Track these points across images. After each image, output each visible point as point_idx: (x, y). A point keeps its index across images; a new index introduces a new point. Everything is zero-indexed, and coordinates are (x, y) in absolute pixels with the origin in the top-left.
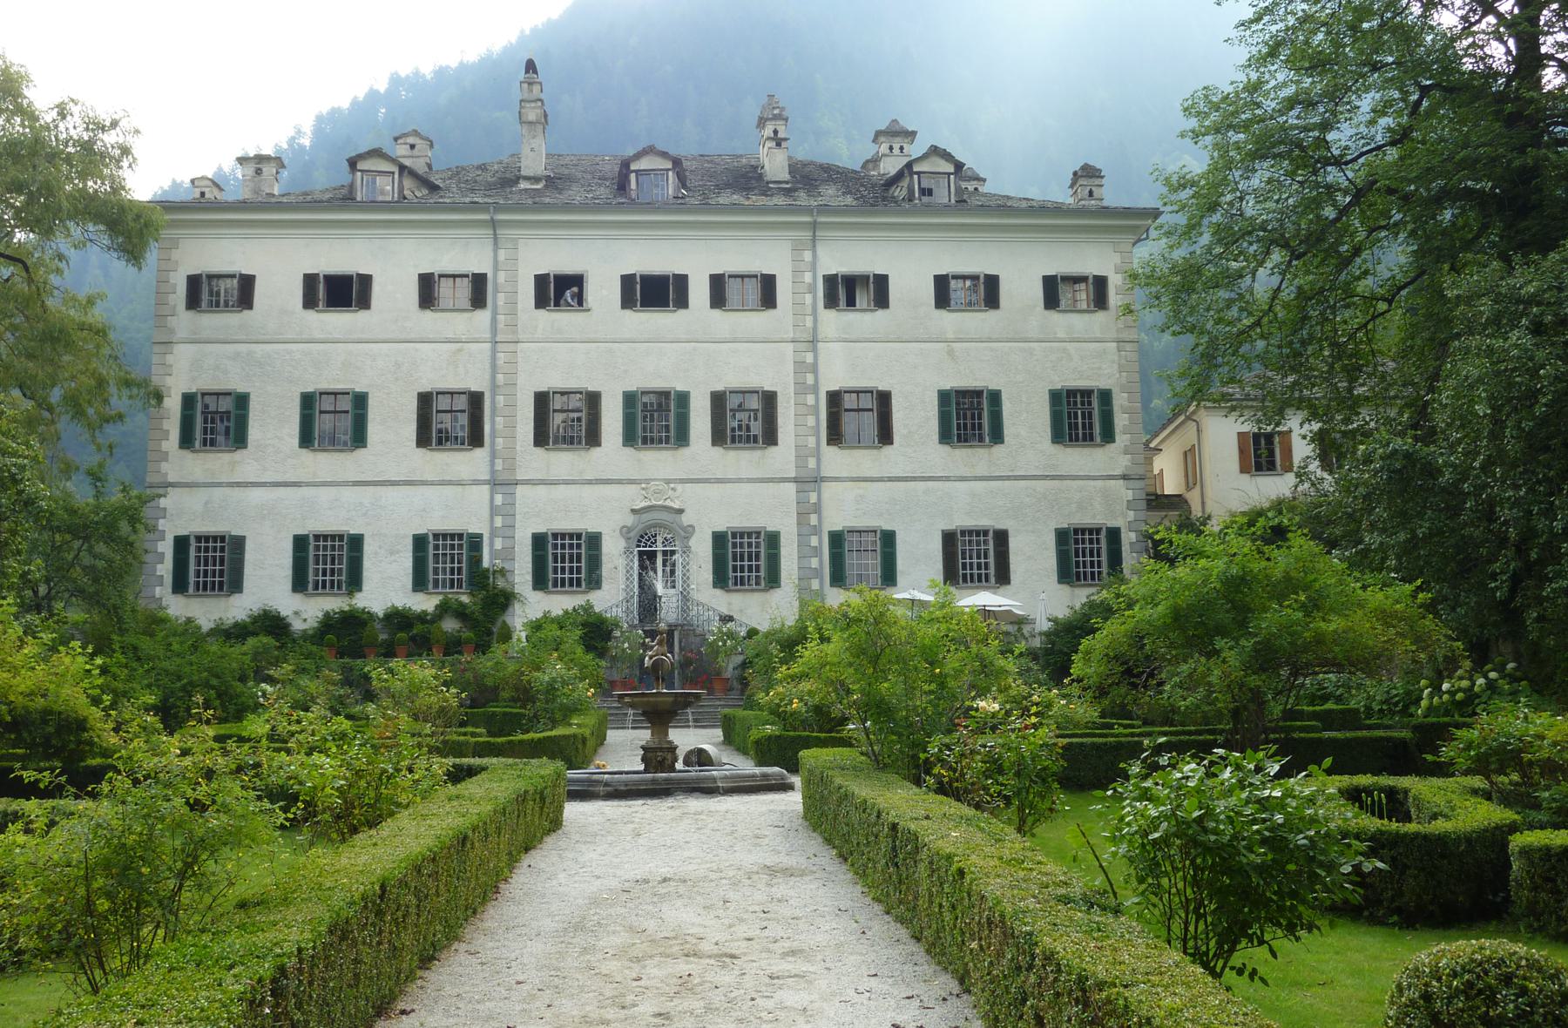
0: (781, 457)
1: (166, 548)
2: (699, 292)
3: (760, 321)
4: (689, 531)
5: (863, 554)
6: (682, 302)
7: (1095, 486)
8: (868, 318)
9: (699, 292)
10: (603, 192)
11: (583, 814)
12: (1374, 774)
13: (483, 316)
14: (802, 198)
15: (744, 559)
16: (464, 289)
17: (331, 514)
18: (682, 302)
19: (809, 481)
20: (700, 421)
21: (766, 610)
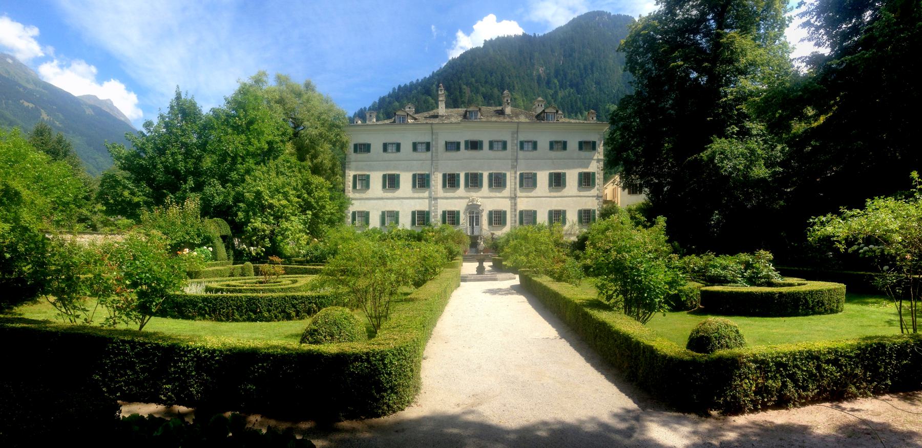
0: (507, 192)
1: (350, 215)
2: (486, 145)
3: (502, 154)
4: (483, 210)
5: (528, 217)
6: (481, 148)
7: (590, 201)
8: (531, 153)
9: (486, 145)
10: (460, 119)
11: (727, 326)
12: (319, 356)
13: (429, 154)
14: (515, 120)
15: (498, 218)
16: (424, 147)
17: (391, 206)
18: (481, 148)
19: (514, 198)
20: (462, 146)
21: (502, 232)
